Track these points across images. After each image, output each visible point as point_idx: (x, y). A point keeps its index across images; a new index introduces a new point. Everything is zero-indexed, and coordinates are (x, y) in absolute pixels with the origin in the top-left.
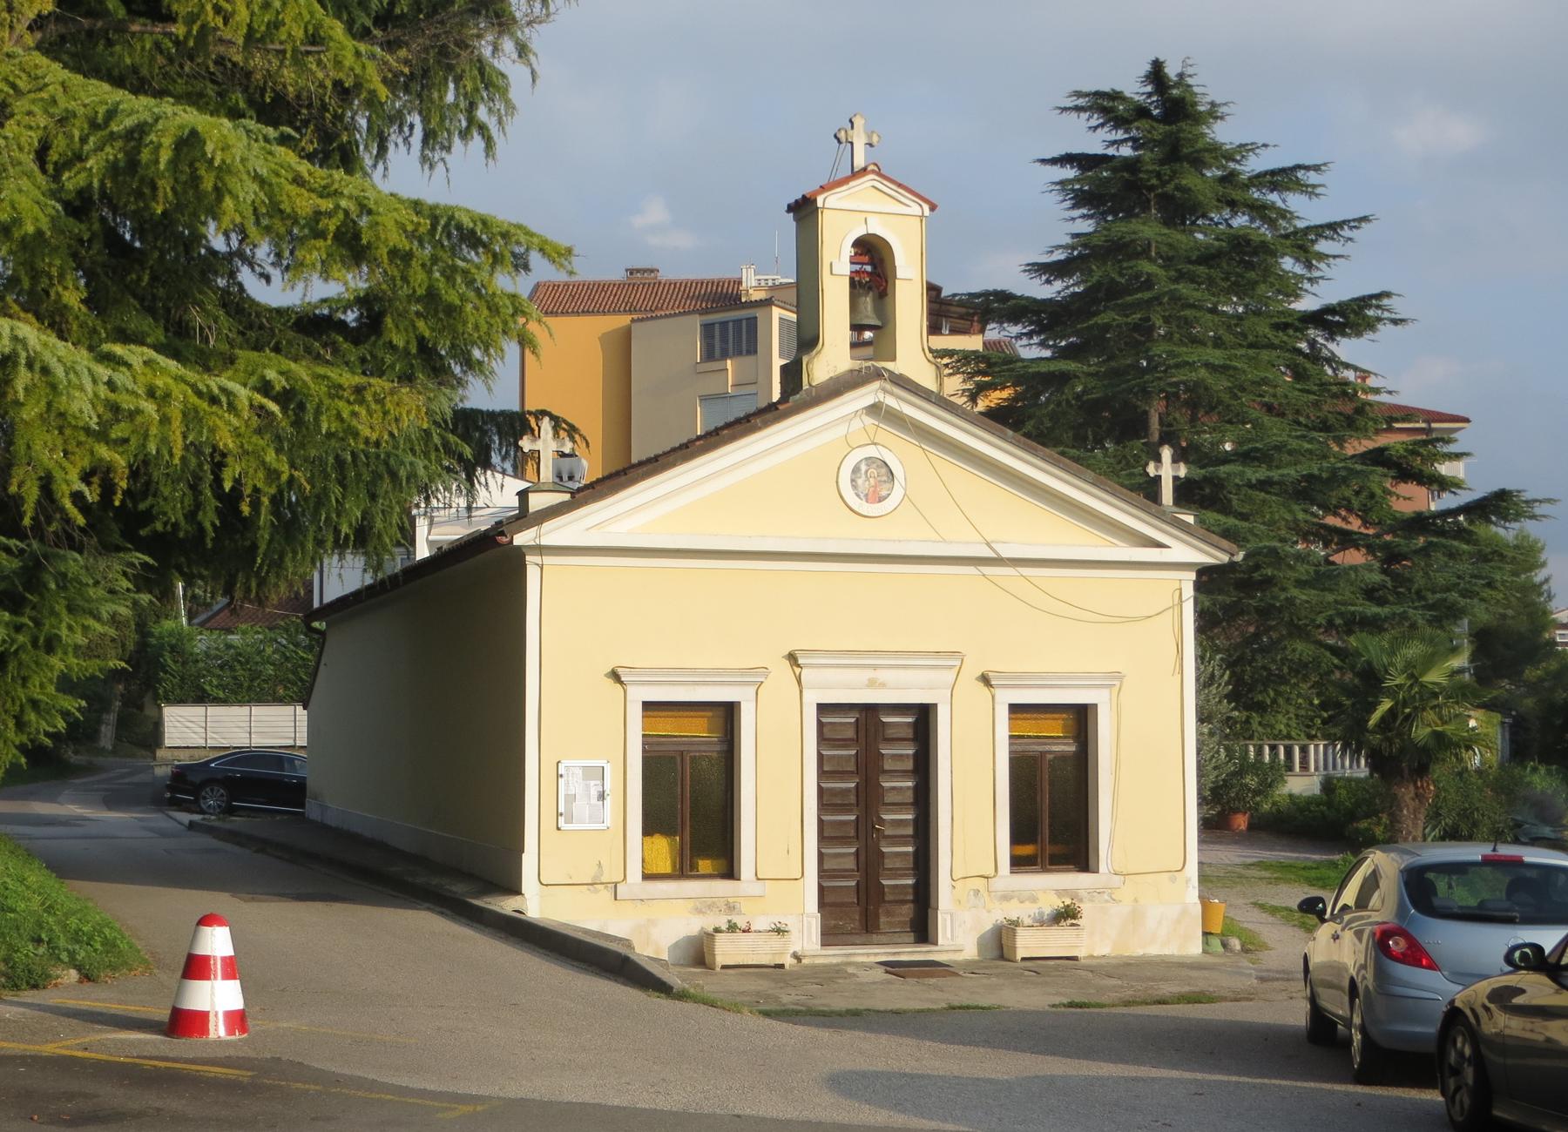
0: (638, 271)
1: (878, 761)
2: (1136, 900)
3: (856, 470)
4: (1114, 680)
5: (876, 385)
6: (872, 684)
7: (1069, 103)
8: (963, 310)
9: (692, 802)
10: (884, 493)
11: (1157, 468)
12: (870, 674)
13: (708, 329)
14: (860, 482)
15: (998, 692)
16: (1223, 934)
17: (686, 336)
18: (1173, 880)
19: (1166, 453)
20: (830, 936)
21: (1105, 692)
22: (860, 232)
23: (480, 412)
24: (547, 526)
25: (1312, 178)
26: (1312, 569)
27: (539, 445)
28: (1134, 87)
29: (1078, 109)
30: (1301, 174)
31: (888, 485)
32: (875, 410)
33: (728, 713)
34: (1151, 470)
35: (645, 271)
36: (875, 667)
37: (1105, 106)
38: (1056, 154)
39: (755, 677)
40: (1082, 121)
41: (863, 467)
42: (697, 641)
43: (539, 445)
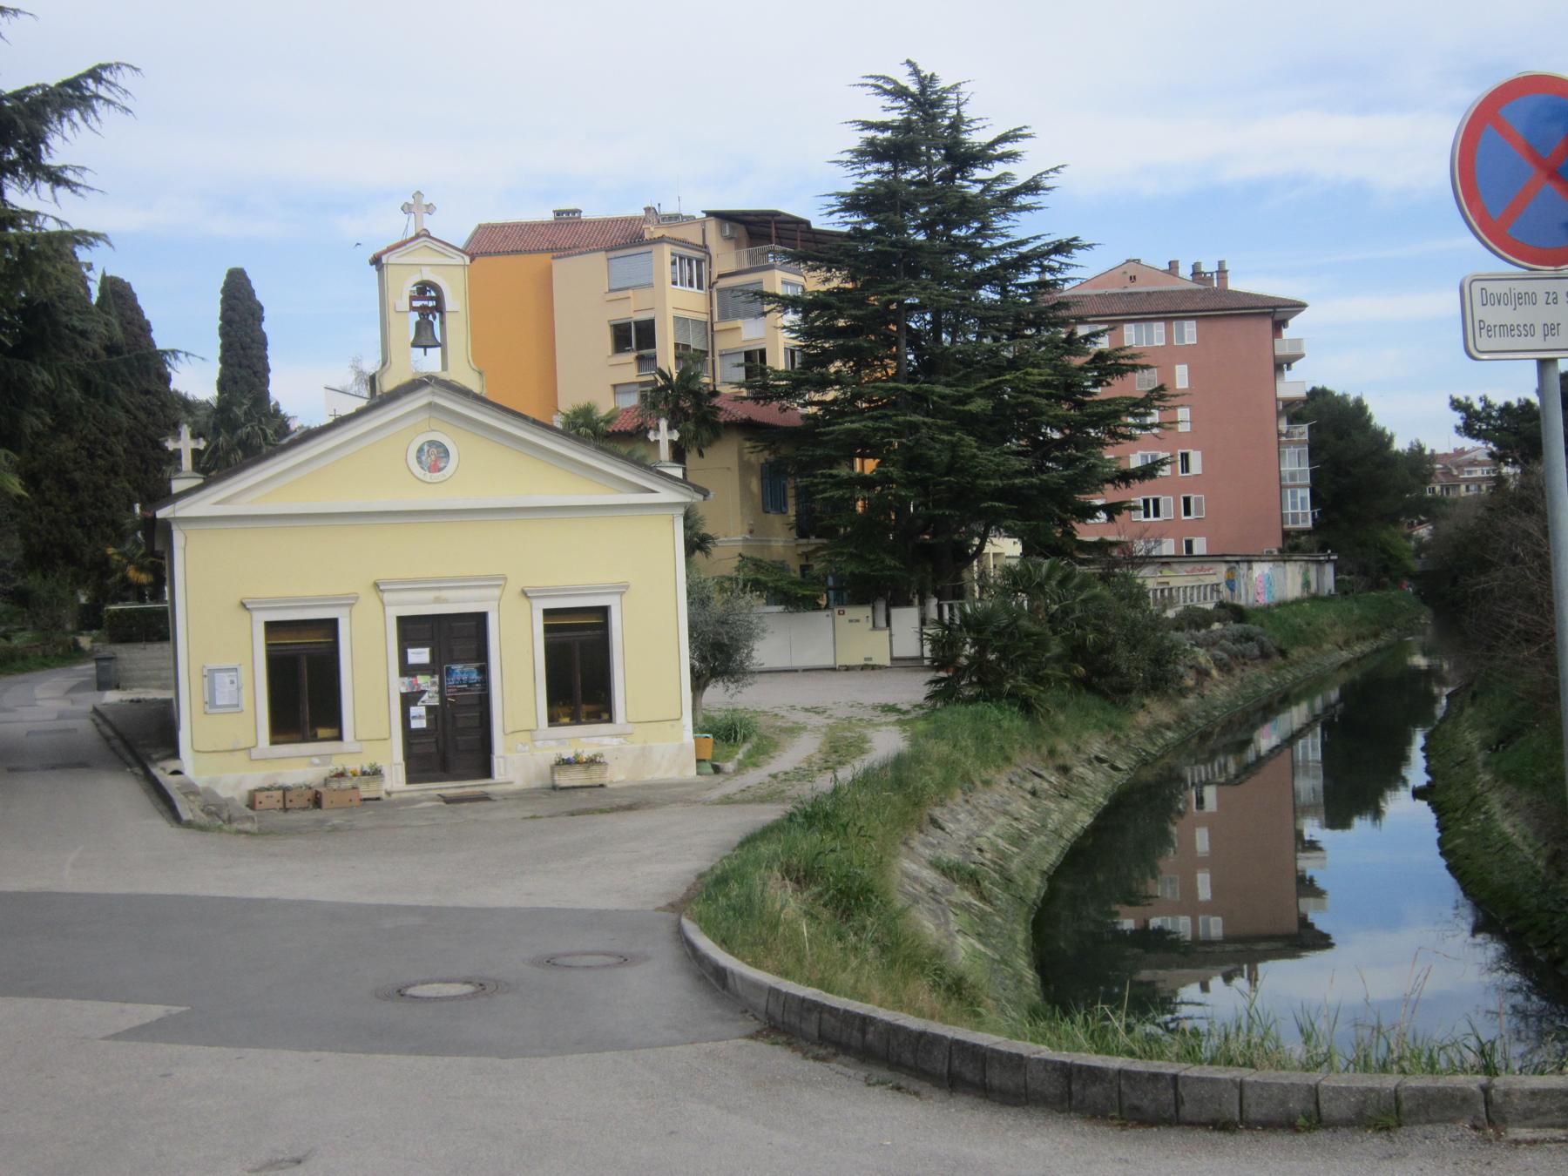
3: (420, 450)
4: (621, 590)
5: (428, 390)
6: (437, 600)
8: (1063, 313)
9: (303, 682)
15: (387, 597)
16: (714, 759)
19: (185, 431)
20: (410, 780)
22: (418, 279)
24: (180, 504)
32: (431, 406)
34: (171, 445)
35: (568, 212)
39: (349, 602)
42: (300, 582)
43: (192, 444)
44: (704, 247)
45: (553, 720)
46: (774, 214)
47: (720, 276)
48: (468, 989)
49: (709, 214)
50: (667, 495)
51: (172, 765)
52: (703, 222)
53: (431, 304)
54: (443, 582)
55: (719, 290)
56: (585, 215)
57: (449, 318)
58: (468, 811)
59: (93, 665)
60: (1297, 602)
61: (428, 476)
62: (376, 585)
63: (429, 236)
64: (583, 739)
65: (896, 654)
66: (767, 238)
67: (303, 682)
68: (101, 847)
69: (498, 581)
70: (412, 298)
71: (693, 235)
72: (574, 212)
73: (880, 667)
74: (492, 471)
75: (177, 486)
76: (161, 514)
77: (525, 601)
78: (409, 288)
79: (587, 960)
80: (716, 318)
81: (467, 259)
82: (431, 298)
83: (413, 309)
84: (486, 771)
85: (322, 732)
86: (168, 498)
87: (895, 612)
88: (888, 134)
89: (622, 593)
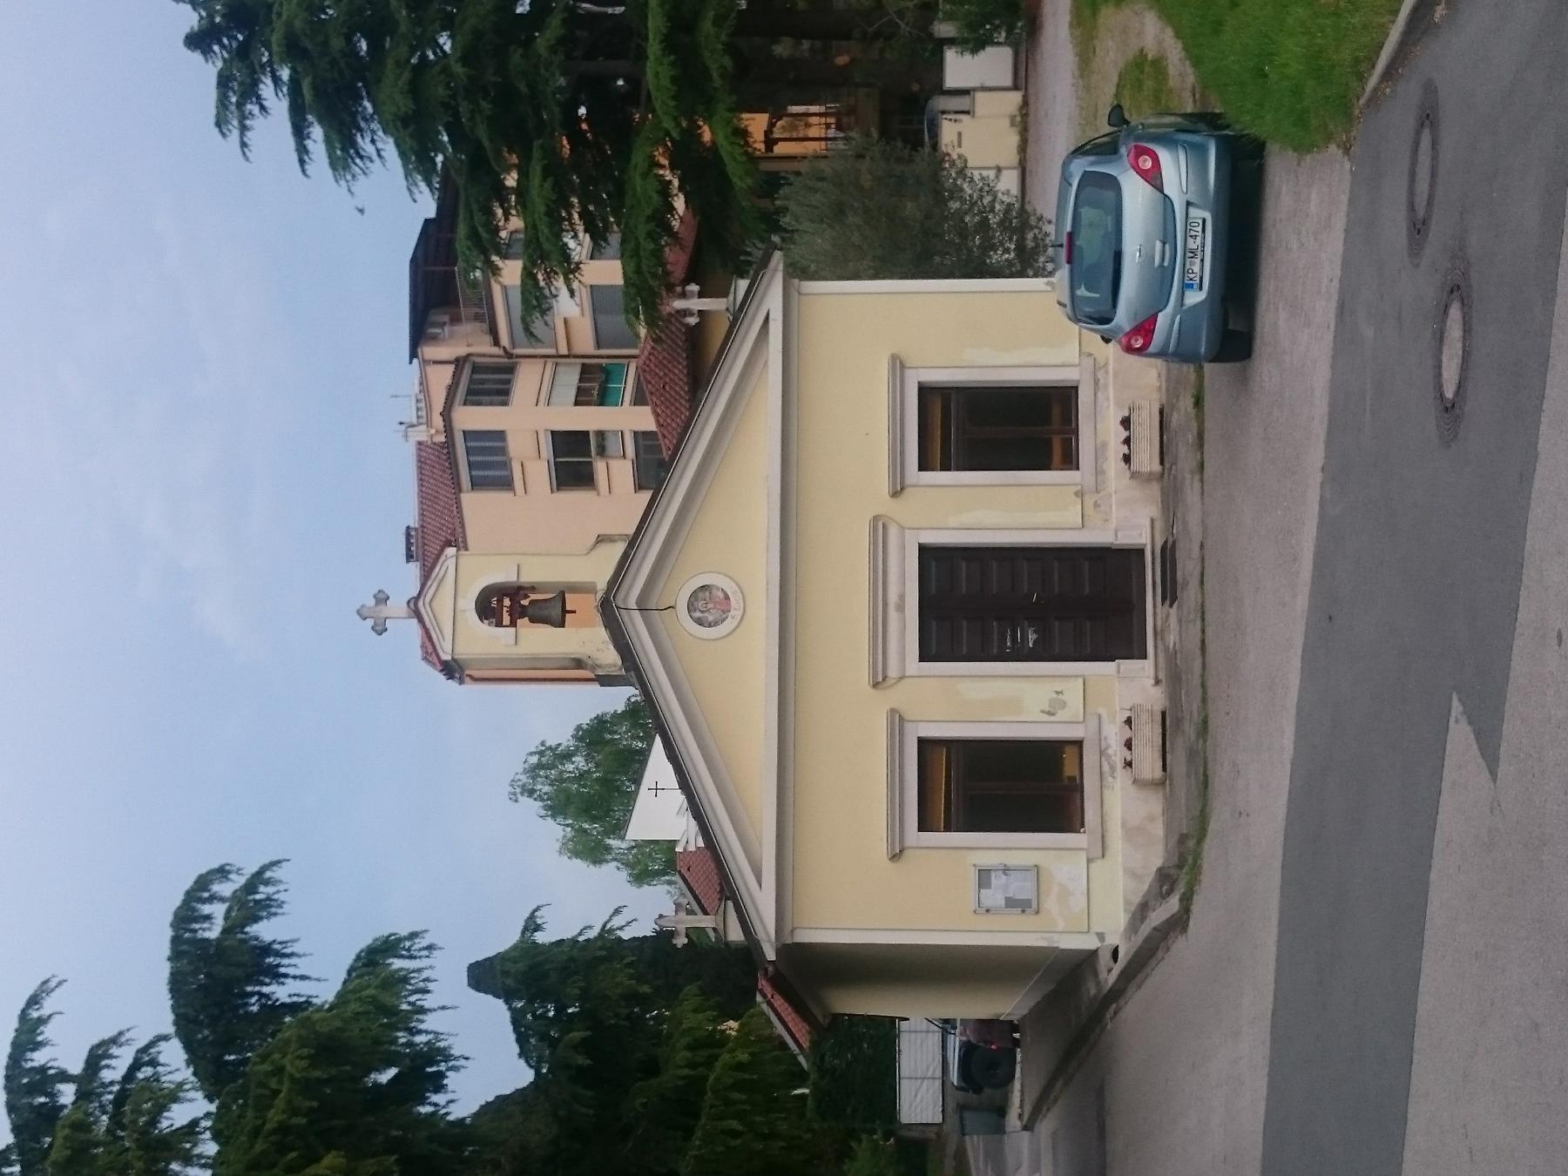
0: (408, 549)
1: (972, 604)
3: (700, 622)
4: (898, 366)
6: (901, 608)
9: (1008, 787)
10: (721, 595)
11: (692, 315)
13: (476, 484)
14: (711, 618)
15: (893, 672)
17: (478, 507)
21: (908, 373)
24: (761, 935)
29: (244, 129)
35: (409, 544)
36: (885, 604)
38: (290, 142)
39: (897, 722)
40: (257, 123)
41: (697, 614)
42: (861, 784)
44: (459, 362)
45: (1070, 460)
46: (414, 261)
47: (496, 343)
48: (1455, 312)
49: (413, 354)
50: (773, 299)
51: (1105, 959)
52: (425, 363)
53: (507, 602)
55: (514, 345)
56: (413, 521)
58: (1187, 567)
59: (967, 1138)
61: (735, 613)
62: (895, 857)
63: (417, 599)
64: (1099, 428)
65: (1008, 82)
66: (449, 278)
67: (1008, 787)
68: (1210, 1076)
69: (879, 527)
70: (499, 624)
71: (442, 377)
72: (408, 536)
73: (1026, 103)
76: (771, 955)
77: (908, 491)
78: (486, 629)
79: (1423, 186)
80: (552, 351)
81: (451, 551)
82: (500, 601)
83: (513, 624)
84: (1140, 552)
85: (1070, 770)
87: (951, 82)
88: (317, 132)
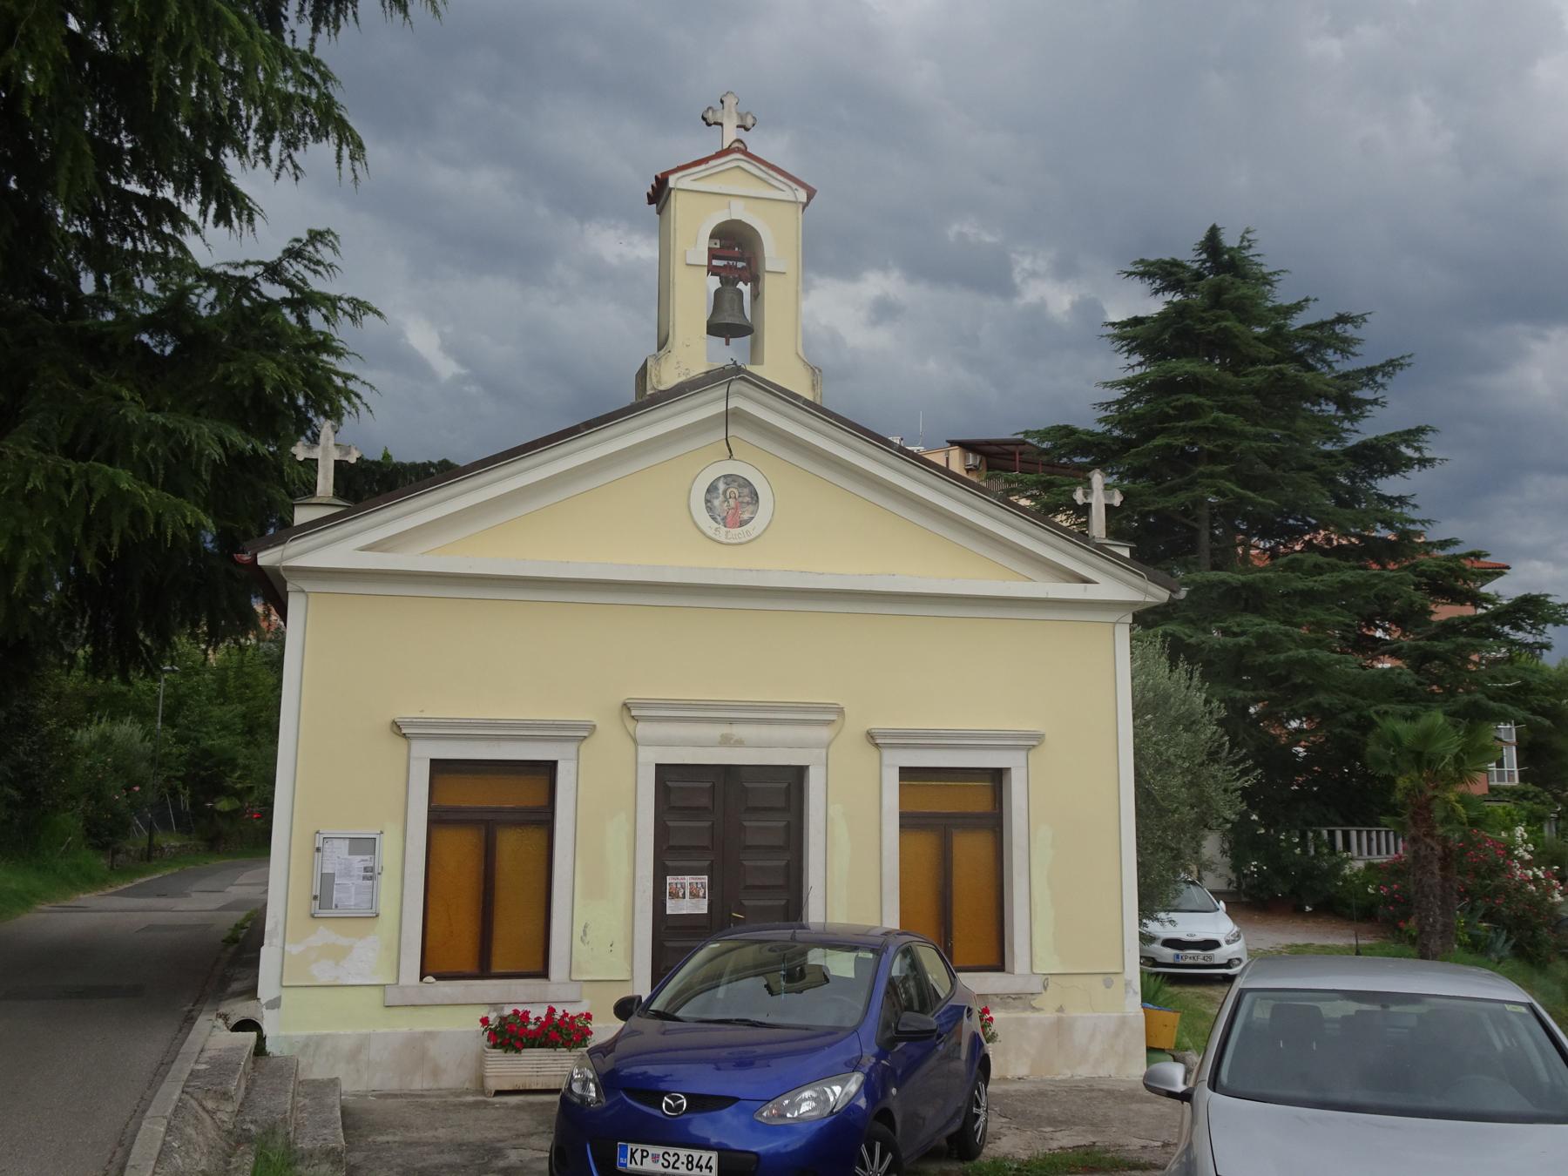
2: (1061, 1009)
3: (712, 489)
4: (1030, 743)
6: (726, 741)
7: (1132, 269)
10: (746, 516)
11: (1086, 495)
12: (724, 729)
14: (716, 503)
15: (642, 729)
18: (1108, 985)
21: (1021, 755)
22: (721, 217)
23: (431, 464)
25: (1349, 330)
26: (303, 45)
27: (317, 453)
28: (1188, 253)
30: (1338, 329)
31: (751, 508)
33: (997, 778)
36: (731, 721)
37: (1164, 274)
41: (721, 486)
42: (495, 686)
54: (733, 695)
57: (769, 285)
60: (794, 909)
61: (722, 533)
63: (745, 152)
69: (831, 715)
74: (818, 531)
75: (302, 516)
83: (713, 271)
86: (287, 531)
89: (1029, 748)
